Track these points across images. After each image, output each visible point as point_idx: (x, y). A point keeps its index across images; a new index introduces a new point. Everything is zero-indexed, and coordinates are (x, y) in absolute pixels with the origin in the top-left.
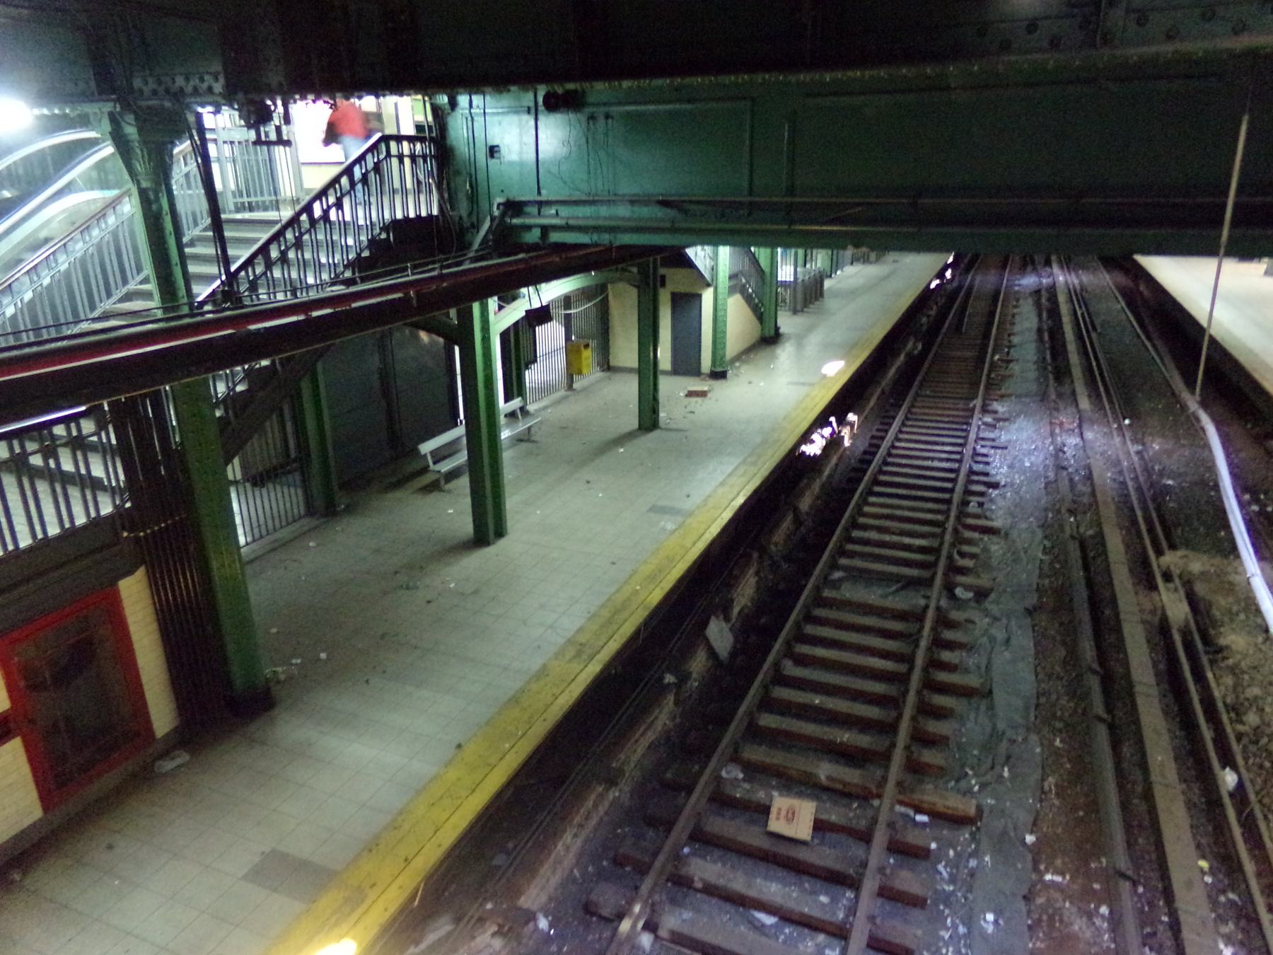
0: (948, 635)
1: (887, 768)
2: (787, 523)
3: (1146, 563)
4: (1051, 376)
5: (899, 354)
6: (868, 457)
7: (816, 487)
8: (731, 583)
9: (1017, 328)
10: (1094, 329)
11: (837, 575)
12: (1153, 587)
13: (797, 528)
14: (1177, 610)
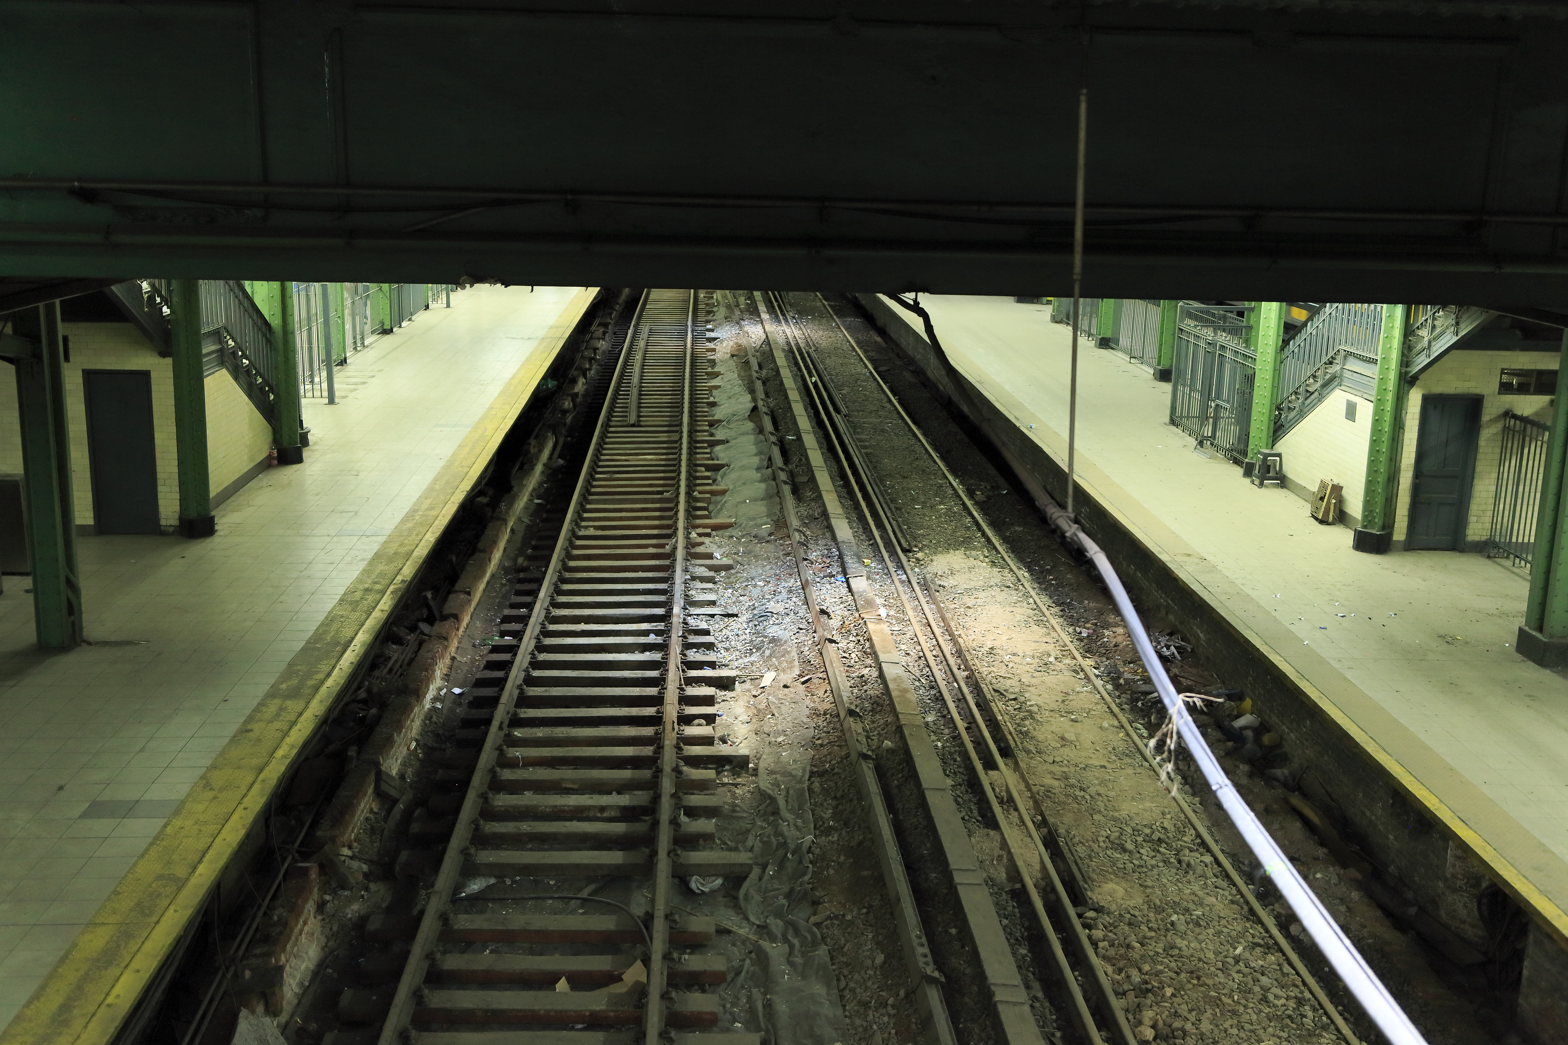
0: (693, 962)
1: (653, 890)
2: (366, 806)
3: (974, 785)
4: (787, 489)
5: (532, 468)
6: (482, 713)
7: (414, 725)
8: (273, 937)
9: (719, 413)
10: (837, 410)
11: (475, 886)
12: (992, 823)
13: (389, 811)
14: (1030, 856)
